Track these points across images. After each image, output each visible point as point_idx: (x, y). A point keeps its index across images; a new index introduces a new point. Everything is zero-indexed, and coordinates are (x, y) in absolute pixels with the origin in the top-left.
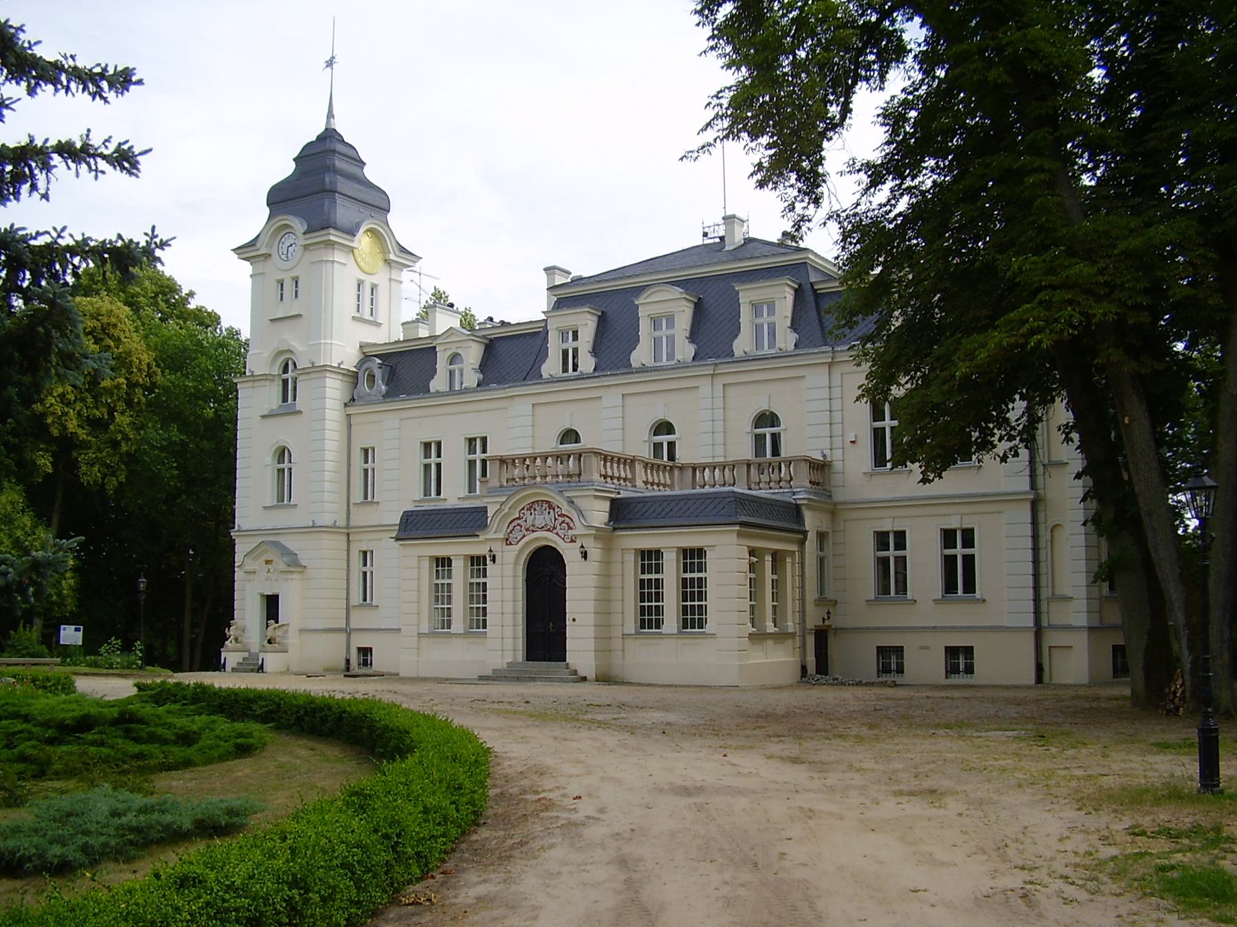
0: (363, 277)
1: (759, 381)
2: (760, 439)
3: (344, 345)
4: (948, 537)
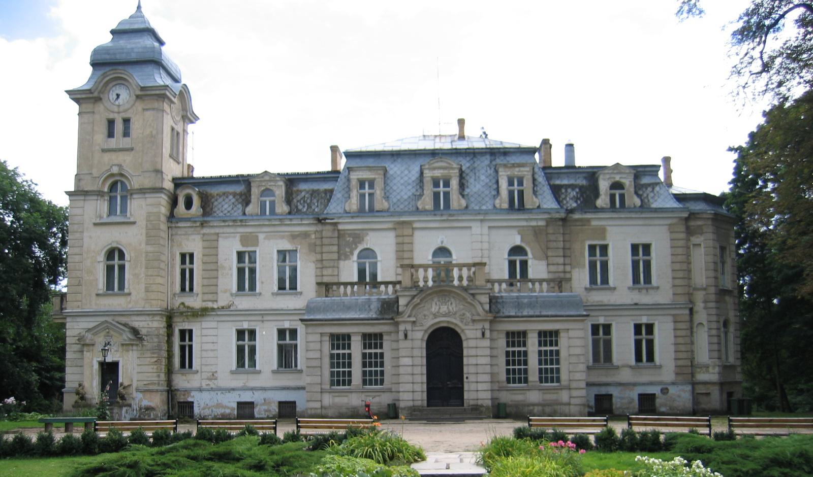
0: (111, 116)
2: (512, 264)
4: (638, 328)
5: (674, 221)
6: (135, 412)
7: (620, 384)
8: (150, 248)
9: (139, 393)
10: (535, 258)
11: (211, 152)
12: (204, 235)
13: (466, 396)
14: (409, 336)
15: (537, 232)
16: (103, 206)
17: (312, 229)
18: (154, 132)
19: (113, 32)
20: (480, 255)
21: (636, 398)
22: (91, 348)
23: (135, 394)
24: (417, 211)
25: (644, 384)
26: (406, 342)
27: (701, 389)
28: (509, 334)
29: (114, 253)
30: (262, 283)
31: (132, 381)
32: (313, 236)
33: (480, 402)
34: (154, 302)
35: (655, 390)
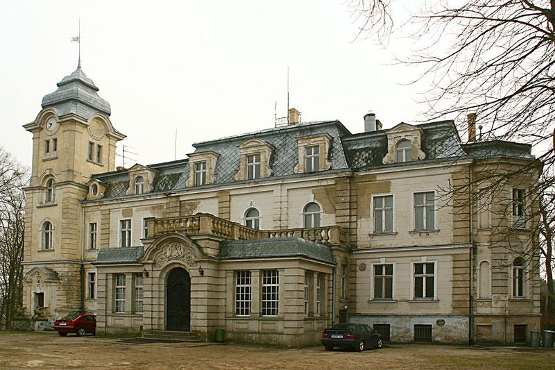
0: (93, 141)
1: (308, 187)
3: (86, 170)
4: (418, 268)
5: (457, 169)
7: (397, 316)
8: (64, 221)
10: (325, 211)
11: (128, 155)
12: (102, 210)
13: (192, 323)
14: (150, 276)
15: (328, 190)
16: (44, 196)
17: (164, 201)
18: (68, 146)
19: (58, 85)
20: (279, 213)
21: (413, 328)
24: (235, 182)
25: (419, 316)
26: (148, 279)
27: (478, 322)
28: (238, 272)
29: (47, 225)
30: (134, 241)
32: (165, 207)
33: (198, 329)
34: (65, 255)
35: (431, 322)
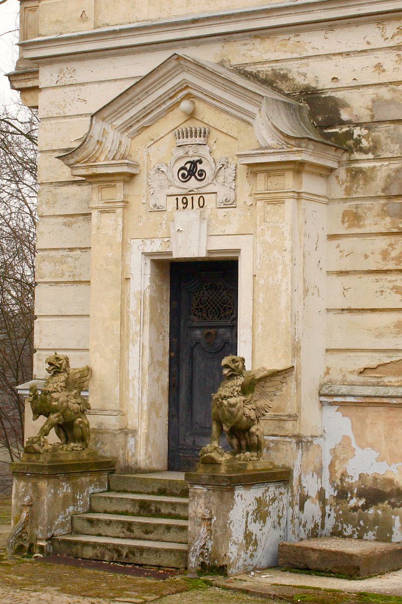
6: (312, 508)
9: (331, 412)
22: (118, 193)
23: (316, 419)
31: (296, 350)
